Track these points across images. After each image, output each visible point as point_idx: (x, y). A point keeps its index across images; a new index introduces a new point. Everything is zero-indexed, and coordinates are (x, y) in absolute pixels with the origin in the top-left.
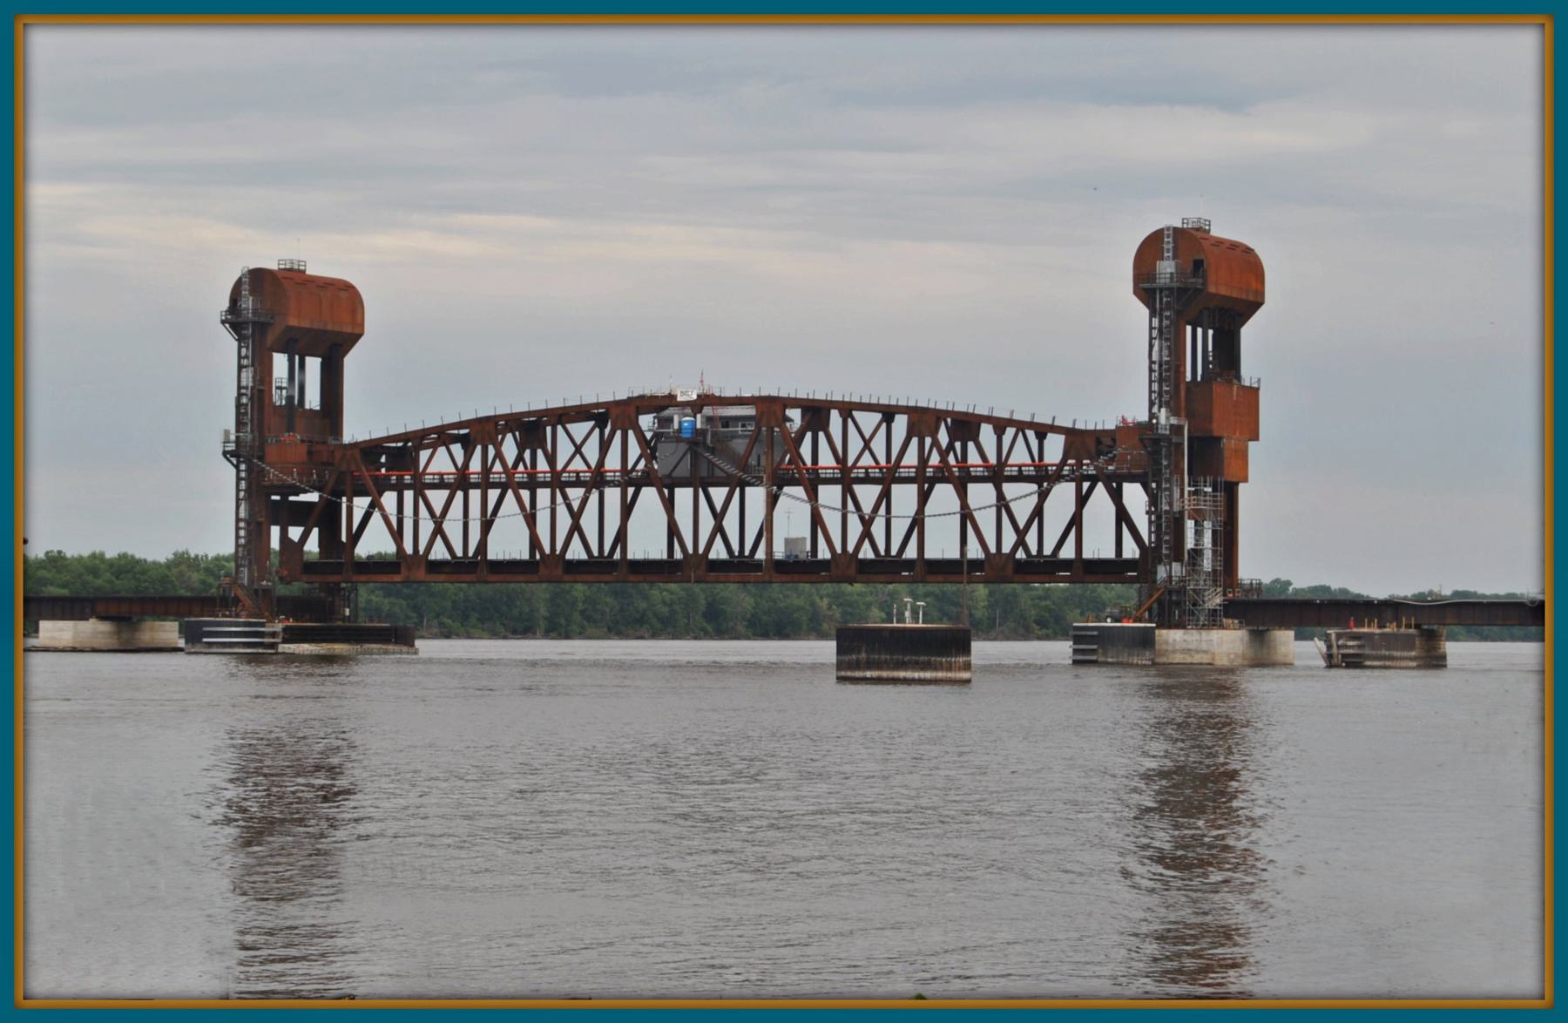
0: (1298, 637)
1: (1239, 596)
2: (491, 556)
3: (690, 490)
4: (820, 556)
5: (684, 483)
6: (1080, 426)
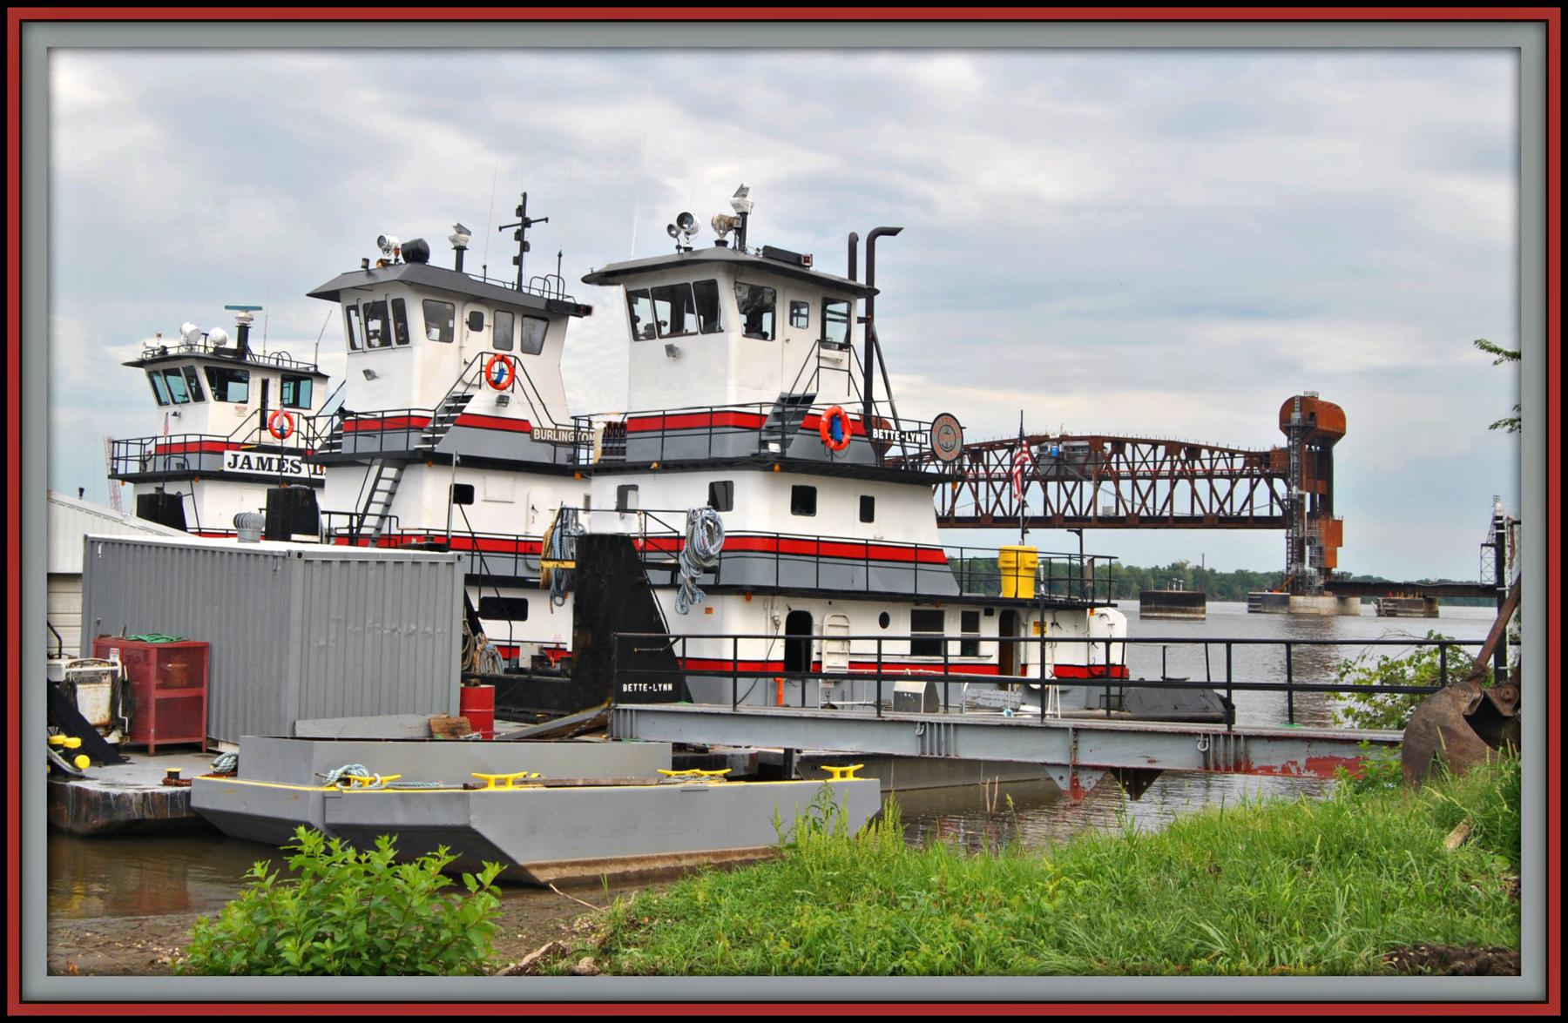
0: (1363, 602)
1: (1333, 580)
2: (956, 515)
3: (1056, 483)
4: (1120, 515)
5: (1052, 479)
6: (1252, 450)
